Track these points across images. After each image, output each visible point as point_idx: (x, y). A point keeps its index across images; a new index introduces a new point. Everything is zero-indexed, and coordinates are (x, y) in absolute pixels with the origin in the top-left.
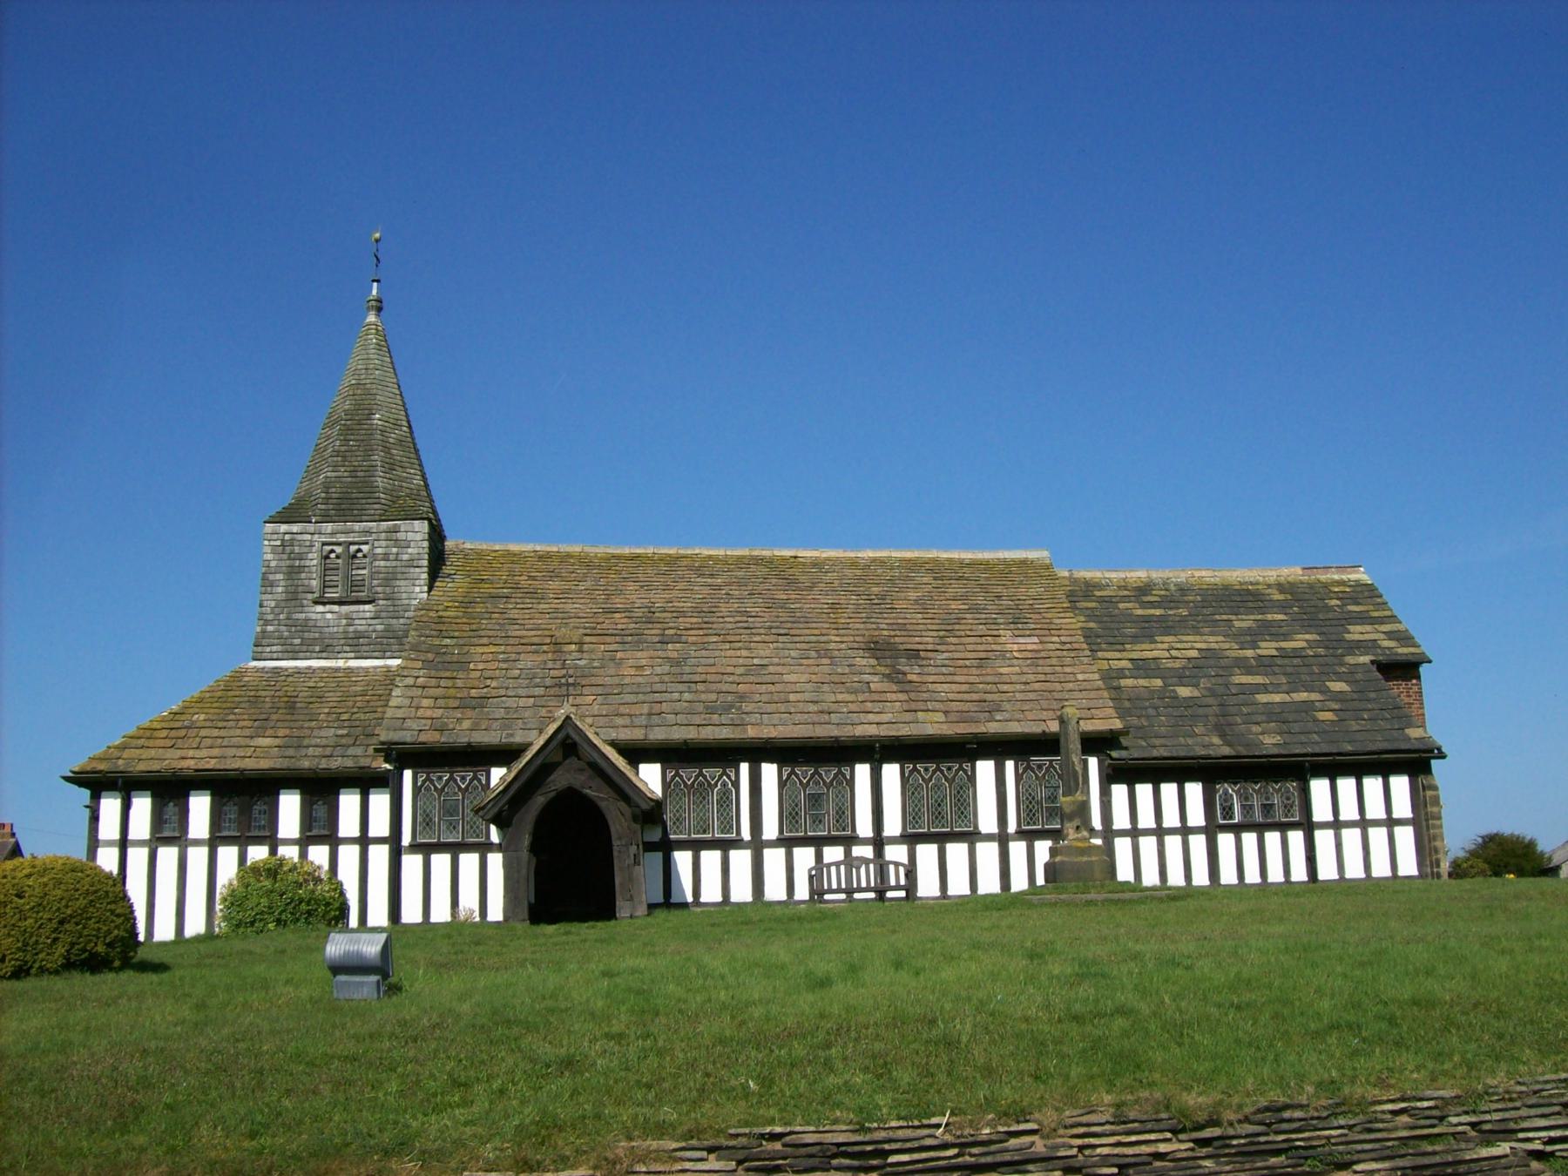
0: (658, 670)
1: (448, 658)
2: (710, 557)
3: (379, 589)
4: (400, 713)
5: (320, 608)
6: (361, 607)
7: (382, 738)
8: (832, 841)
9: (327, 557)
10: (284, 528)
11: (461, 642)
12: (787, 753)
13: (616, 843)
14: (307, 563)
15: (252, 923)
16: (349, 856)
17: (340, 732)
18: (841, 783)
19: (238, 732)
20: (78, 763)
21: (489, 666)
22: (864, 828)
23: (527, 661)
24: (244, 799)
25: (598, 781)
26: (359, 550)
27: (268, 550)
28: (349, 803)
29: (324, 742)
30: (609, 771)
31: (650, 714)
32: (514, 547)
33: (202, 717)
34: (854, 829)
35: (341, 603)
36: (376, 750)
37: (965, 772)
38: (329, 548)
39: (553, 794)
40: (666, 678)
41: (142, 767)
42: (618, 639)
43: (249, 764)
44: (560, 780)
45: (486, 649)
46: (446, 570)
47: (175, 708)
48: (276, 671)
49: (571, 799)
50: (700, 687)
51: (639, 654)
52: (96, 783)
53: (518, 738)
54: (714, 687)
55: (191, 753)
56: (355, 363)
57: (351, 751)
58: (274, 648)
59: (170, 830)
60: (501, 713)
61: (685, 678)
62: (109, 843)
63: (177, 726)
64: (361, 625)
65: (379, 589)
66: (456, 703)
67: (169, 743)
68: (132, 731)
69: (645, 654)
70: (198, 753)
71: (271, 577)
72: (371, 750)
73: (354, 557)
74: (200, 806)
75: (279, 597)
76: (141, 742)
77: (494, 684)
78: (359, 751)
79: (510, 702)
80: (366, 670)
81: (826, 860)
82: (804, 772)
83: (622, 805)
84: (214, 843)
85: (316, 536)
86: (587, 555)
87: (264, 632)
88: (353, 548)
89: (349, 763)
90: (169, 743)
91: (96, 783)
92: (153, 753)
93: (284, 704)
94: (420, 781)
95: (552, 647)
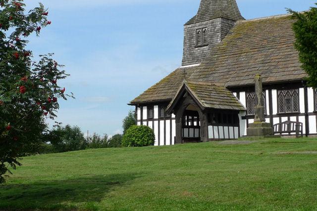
5: (197, 49)
8: (293, 115)
12: (279, 86)
16: (156, 123)
18: (295, 95)
20: (132, 98)
22: (302, 110)
30: (199, 104)
34: (299, 111)
37: (296, 92)
81: (282, 121)
82: (284, 92)
84: (160, 119)
88: (204, 29)
94: (247, 95)
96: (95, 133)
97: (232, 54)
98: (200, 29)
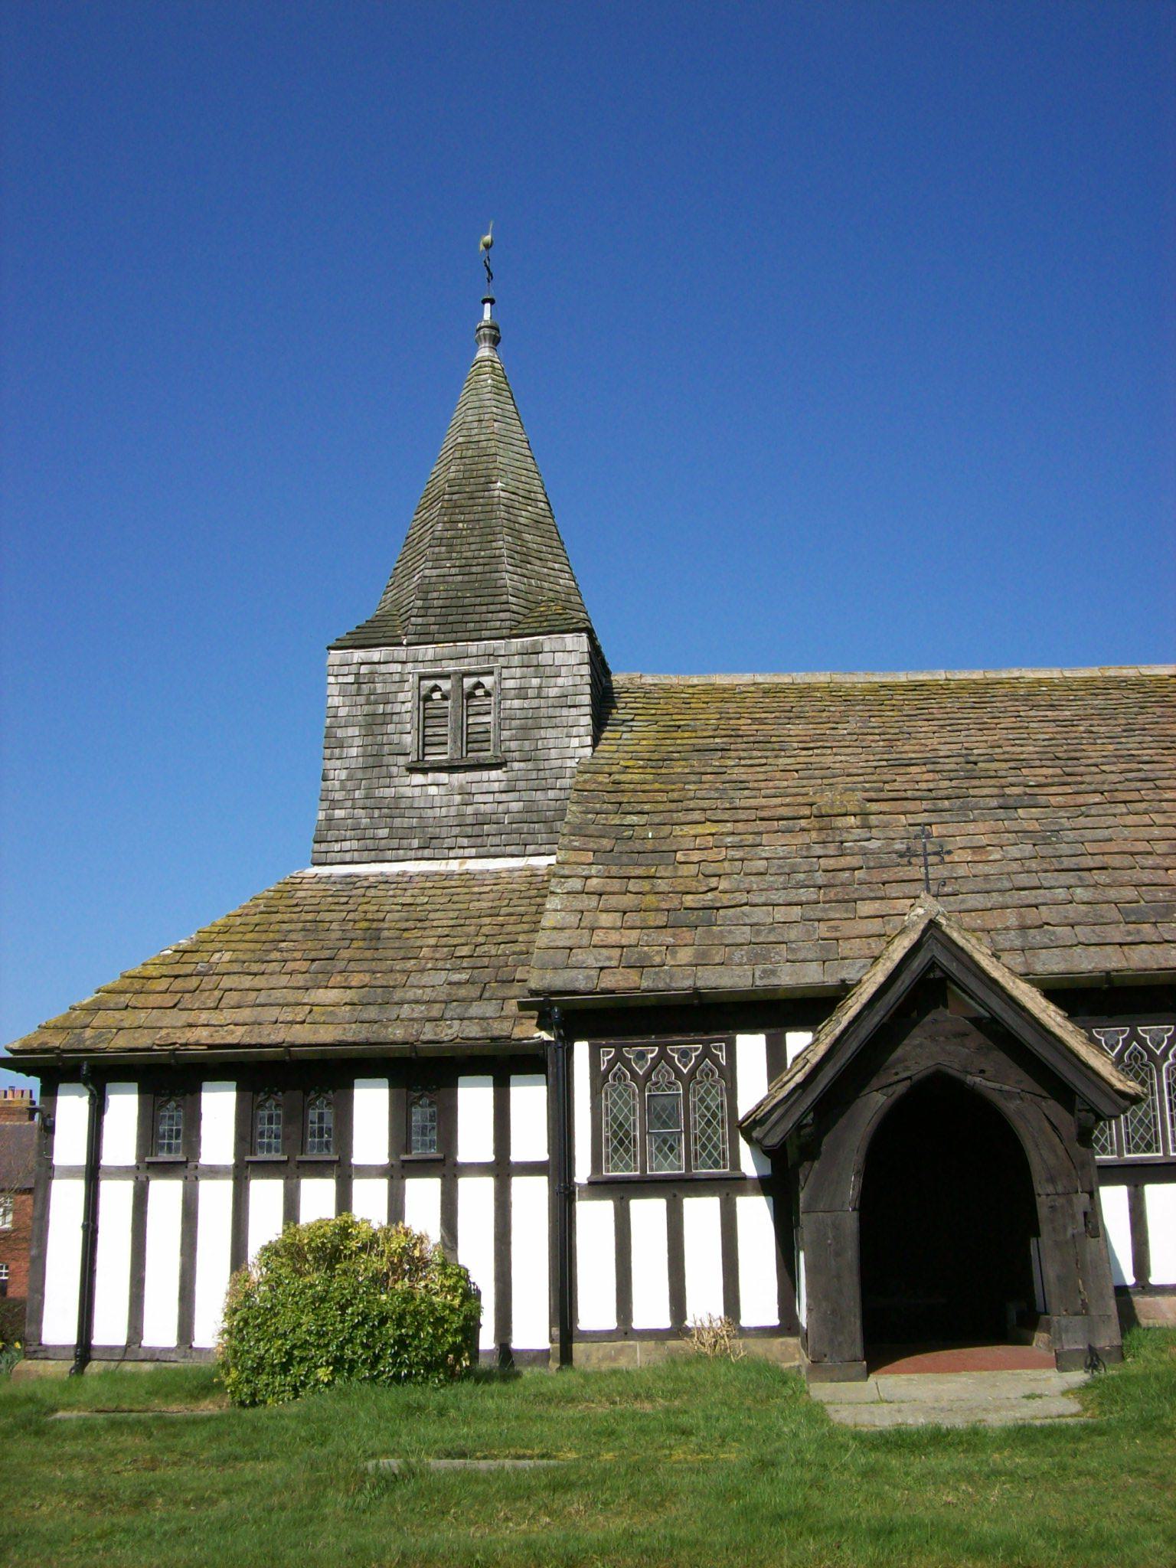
0: (1014, 852)
1: (637, 845)
2: (1039, 682)
3: (513, 745)
4: (563, 939)
5: (418, 779)
6: (485, 775)
7: (533, 985)
9: (427, 698)
10: (358, 655)
11: (657, 819)
13: (1042, 1189)
14: (397, 708)
15: (285, 1368)
16: (476, 1195)
17: (456, 977)
19: (284, 980)
21: (711, 855)
23: (776, 846)
24: (293, 1095)
25: (1000, 1057)
26: (479, 685)
27: (333, 690)
28: (474, 1100)
29: (428, 994)
30: (1029, 1037)
31: (1023, 928)
32: (721, 680)
33: (227, 956)
35: (451, 769)
36: (523, 1006)
37: (715, 1059)
38: (431, 683)
39: (901, 1089)
40: (1033, 865)
41: (121, 1041)
42: (925, 805)
43: (302, 1035)
44: (918, 1055)
45: (699, 829)
46: (617, 715)
47: (184, 943)
48: (350, 881)
49: (939, 1100)
50: (1101, 877)
51: (971, 828)
52: (53, 1068)
53: (849, 974)
54: (1126, 876)
55: (204, 1017)
56: (464, 414)
57: (475, 1010)
58: (347, 845)
59: (168, 1150)
60: (744, 934)
61: (1067, 863)
62: (70, 1172)
63: (185, 975)
64: (485, 804)
65: (513, 745)
66: (662, 919)
67: (169, 999)
68: (112, 981)
69: (981, 827)
70: (216, 1018)
71: (340, 733)
72: (512, 1007)
73: (471, 695)
74: (219, 1108)
75: (353, 763)
76: (124, 999)
77: (724, 884)
78: (489, 1009)
79: (759, 915)
80: (496, 874)
83: (1052, 1107)
84: (242, 1172)
85: (406, 668)
86: (841, 685)
87: (329, 819)
88: (468, 682)
89: (473, 1030)
90: (169, 999)
91: (53, 1068)
92: (142, 1017)
93: (365, 933)
95: (815, 822)
96: (560, 1369)
97: (788, 800)
98: (446, 676)
